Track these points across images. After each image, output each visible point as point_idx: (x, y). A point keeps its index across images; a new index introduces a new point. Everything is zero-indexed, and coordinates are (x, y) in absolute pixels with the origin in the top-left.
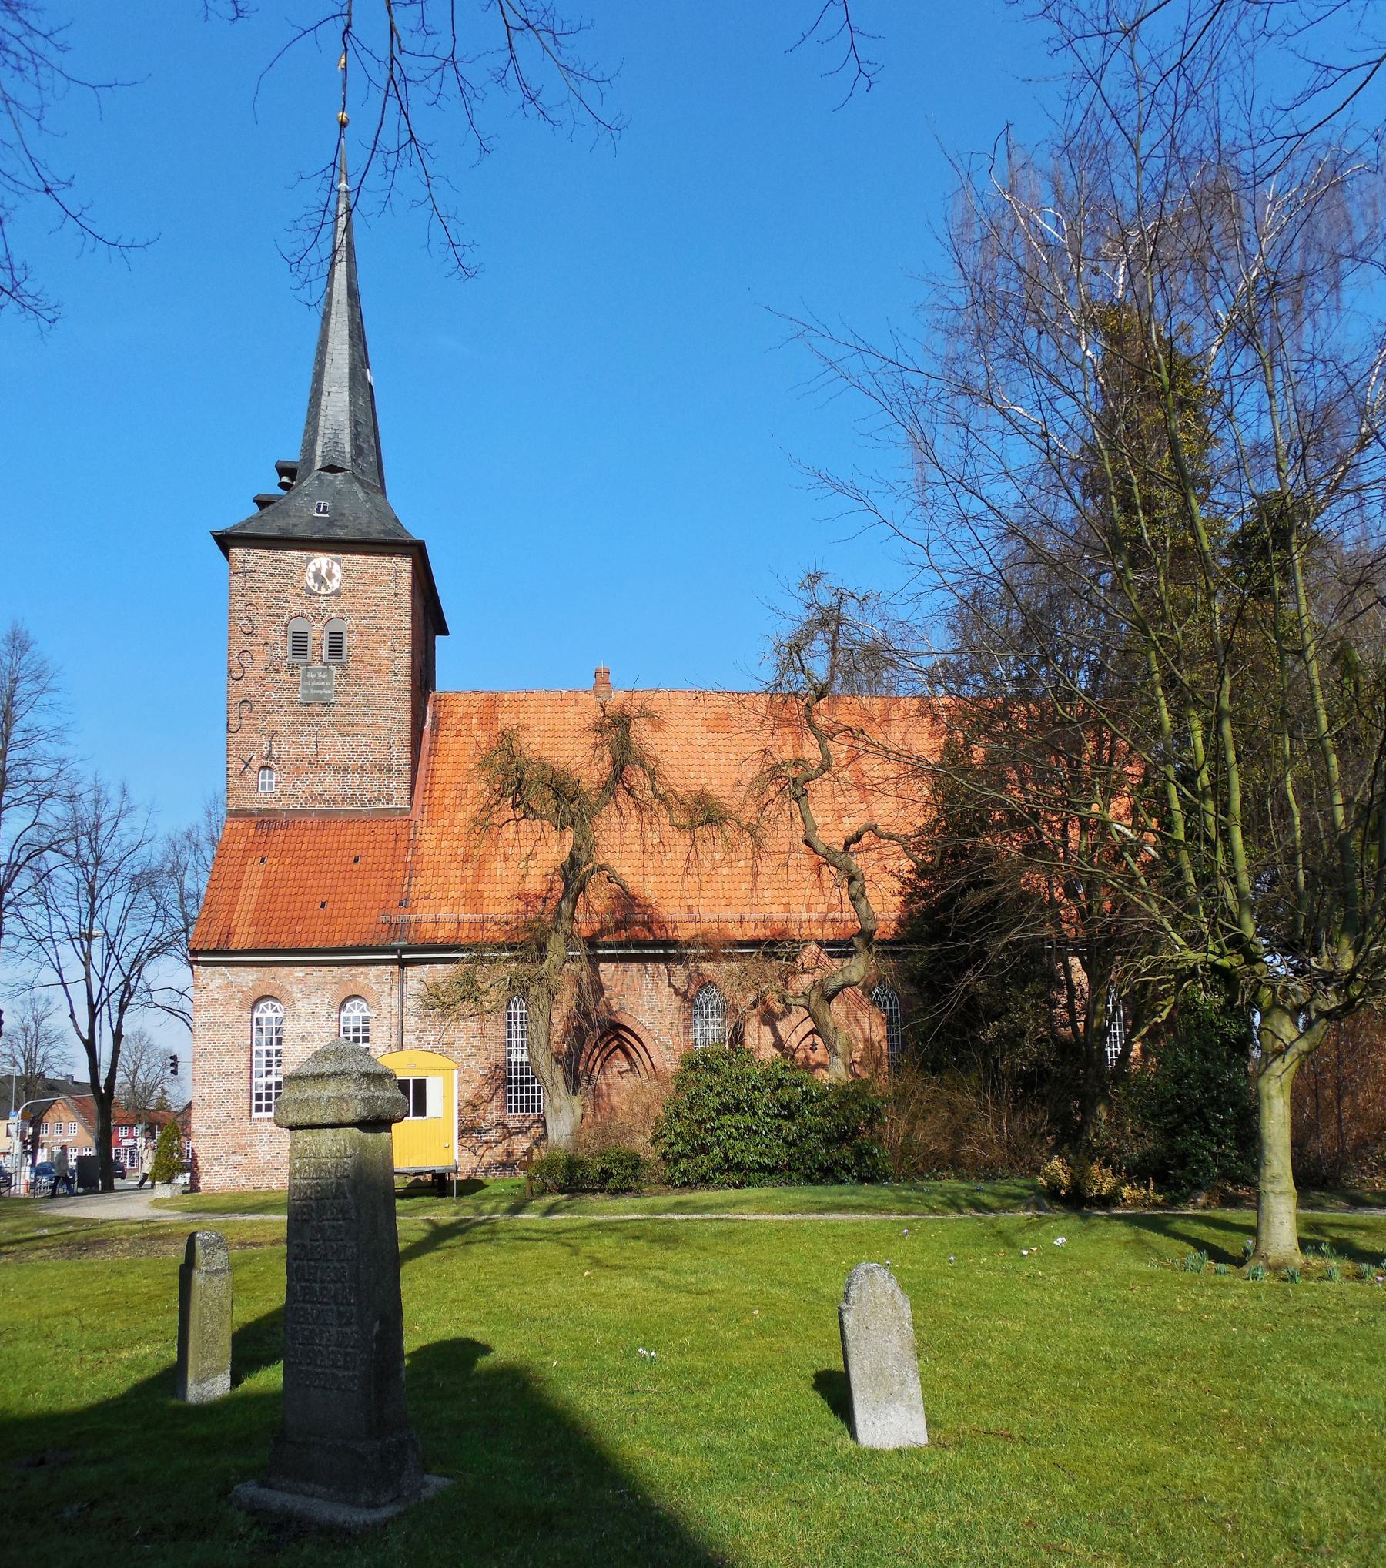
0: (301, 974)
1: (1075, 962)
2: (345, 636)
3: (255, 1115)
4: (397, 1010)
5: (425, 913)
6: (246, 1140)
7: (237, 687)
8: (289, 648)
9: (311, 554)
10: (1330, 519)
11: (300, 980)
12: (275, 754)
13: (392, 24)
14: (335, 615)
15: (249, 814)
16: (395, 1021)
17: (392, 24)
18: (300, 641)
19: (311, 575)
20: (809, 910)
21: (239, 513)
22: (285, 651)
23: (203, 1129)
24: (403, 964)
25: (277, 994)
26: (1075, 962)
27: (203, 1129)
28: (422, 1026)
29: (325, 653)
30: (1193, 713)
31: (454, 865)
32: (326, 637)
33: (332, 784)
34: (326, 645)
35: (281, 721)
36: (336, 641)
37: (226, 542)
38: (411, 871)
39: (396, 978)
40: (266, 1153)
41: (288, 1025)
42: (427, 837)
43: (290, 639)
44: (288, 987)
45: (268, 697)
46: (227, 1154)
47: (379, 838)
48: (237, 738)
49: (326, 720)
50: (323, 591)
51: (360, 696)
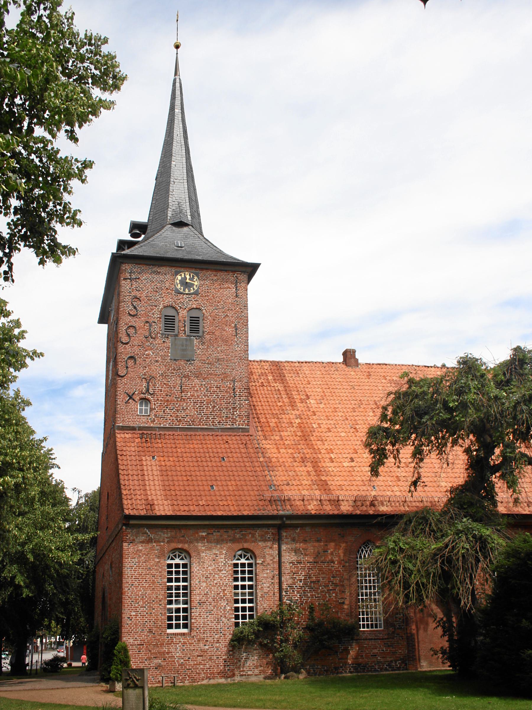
0: (204, 534)
2: (201, 319)
4: (277, 559)
7: (125, 348)
8: (162, 325)
9: (178, 269)
13: (177, 57)
14: (195, 306)
15: (133, 429)
16: (276, 566)
17: (177, 57)
18: (169, 322)
19: (178, 282)
21: (57, 469)
22: (159, 327)
23: (131, 641)
24: (280, 528)
27: (131, 641)
29: (187, 329)
30: (478, 423)
31: (295, 464)
32: (187, 320)
34: (188, 324)
36: (195, 324)
37: (59, 468)
42: (268, 446)
43: (163, 320)
45: (148, 355)
50: (187, 291)
51: (213, 356)
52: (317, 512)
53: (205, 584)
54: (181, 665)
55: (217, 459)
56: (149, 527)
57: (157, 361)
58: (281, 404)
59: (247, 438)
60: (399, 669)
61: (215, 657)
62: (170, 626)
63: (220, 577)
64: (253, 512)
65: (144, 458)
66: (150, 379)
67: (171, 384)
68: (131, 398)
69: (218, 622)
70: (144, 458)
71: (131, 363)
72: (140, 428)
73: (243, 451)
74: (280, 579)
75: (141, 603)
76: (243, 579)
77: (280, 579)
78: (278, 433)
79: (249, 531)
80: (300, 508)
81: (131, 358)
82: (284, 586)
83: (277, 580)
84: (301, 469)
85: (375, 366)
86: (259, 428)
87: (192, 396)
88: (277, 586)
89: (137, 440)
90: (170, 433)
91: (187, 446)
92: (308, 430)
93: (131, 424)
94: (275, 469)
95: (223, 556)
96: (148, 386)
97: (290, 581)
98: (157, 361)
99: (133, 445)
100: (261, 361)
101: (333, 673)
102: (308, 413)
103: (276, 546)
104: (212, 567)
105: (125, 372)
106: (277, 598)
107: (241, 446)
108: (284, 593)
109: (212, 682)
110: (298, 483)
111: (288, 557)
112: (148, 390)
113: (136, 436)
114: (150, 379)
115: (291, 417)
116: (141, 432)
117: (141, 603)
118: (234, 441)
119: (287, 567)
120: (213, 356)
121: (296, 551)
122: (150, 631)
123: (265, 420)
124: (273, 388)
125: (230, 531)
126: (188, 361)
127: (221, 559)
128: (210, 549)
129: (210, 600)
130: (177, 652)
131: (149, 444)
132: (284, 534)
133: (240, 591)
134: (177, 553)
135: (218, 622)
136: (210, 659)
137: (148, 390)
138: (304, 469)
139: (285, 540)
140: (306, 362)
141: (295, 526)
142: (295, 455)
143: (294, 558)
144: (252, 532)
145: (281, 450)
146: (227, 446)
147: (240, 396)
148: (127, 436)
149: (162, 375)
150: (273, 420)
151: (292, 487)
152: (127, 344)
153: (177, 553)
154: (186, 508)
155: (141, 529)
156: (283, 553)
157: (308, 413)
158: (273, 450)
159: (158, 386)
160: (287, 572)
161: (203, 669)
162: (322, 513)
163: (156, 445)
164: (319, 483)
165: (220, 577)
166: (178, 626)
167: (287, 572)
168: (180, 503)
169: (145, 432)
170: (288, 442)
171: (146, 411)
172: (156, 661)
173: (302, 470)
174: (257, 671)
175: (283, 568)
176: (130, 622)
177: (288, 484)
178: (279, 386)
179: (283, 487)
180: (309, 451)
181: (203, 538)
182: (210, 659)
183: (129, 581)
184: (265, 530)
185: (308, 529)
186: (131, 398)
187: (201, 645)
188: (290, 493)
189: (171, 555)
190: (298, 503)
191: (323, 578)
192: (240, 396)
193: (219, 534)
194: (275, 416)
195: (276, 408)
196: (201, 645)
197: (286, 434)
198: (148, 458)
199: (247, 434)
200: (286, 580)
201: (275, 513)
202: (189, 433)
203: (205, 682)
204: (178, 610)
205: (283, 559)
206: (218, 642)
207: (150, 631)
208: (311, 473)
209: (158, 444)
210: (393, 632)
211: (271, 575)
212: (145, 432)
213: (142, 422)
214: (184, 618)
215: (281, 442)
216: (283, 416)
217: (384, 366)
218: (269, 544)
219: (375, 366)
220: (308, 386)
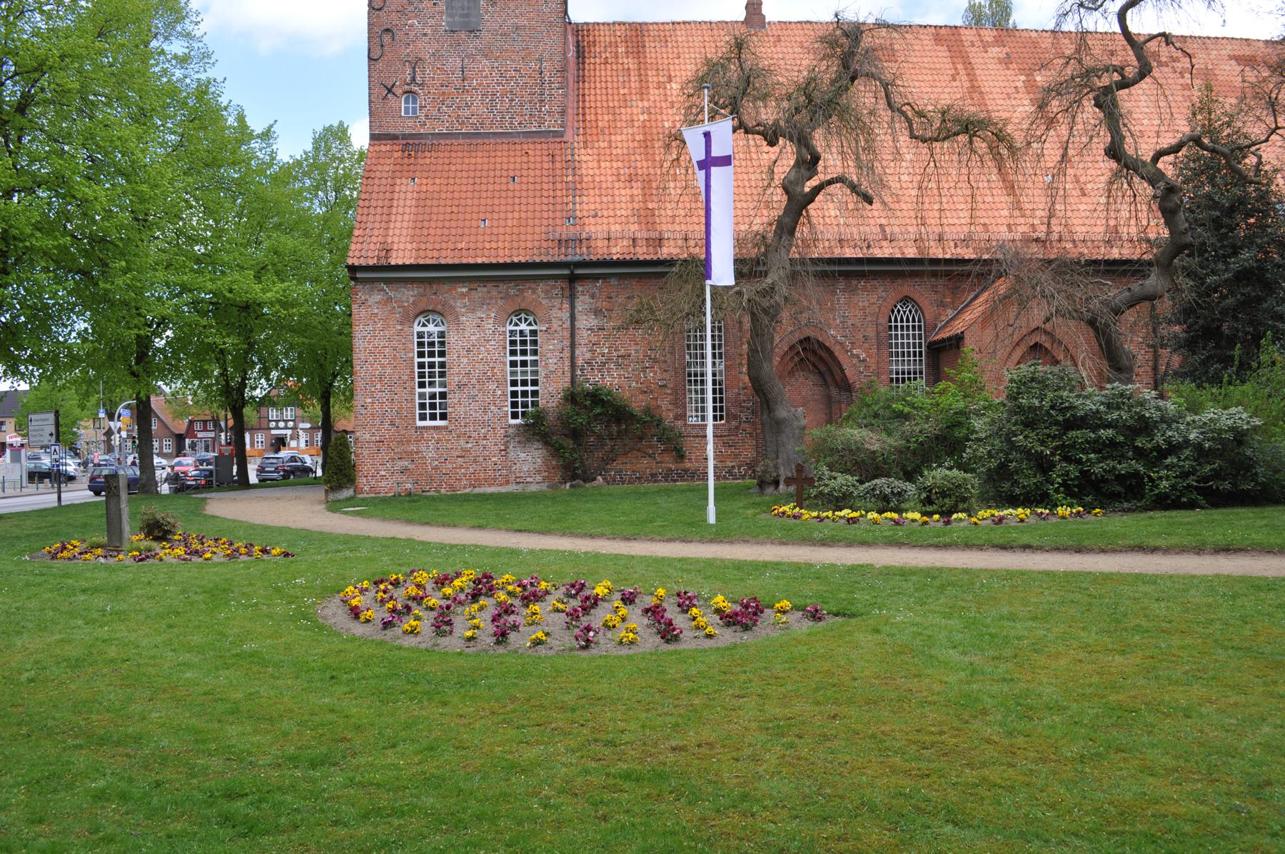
0: (464, 290)
1: (712, 519)
3: (420, 423)
4: (568, 324)
5: (594, 229)
6: (413, 448)
7: (378, 16)
10: (121, 472)
11: (463, 295)
12: (418, 79)
15: (394, 137)
16: (567, 334)
20: (1010, 231)
23: (367, 436)
24: (573, 279)
25: (439, 307)
26: (712, 519)
27: (367, 436)
28: (594, 339)
31: (617, 185)
33: (479, 107)
35: (425, 49)
38: (575, 189)
39: (567, 293)
40: (433, 459)
41: (452, 338)
44: (452, 302)
46: (393, 460)
47: (532, 159)
48: (380, 65)
49: (472, 45)
52: (621, 257)
53: (466, 360)
54: (436, 468)
55: (504, 180)
56: (388, 281)
57: (425, 35)
58: (626, 91)
59: (558, 146)
60: (743, 477)
61: (481, 459)
62: (423, 417)
63: (488, 352)
64: (528, 258)
65: (398, 181)
66: (416, 63)
67: (448, 67)
68: (390, 91)
69: (485, 412)
70: (398, 181)
71: (387, 39)
72: (405, 136)
73: (546, 166)
74: (573, 353)
75: (378, 386)
76: (524, 353)
77: (573, 353)
78: (607, 138)
79: (528, 285)
80: (601, 251)
81: (387, 30)
82: (580, 362)
83: (567, 354)
84: (623, 192)
85: (794, 26)
86: (581, 131)
87: (480, 85)
88: (567, 363)
89: (396, 155)
90: (448, 142)
91: (467, 161)
92: (655, 131)
93: (392, 131)
94: (585, 193)
95: (491, 321)
96: (414, 72)
97: (588, 355)
98: (425, 35)
99: (388, 161)
100: (614, 23)
101: (649, 481)
102: (664, 105)
103: (566, 306)
104: (477, 337)
105: (379, 53)
106: (568, 379)
107: (546, 159)
108: (579, 372)
109: (477, 490)
110: (611, 213)
111: (584, 322)
112: (414, 79)
113: (397, 148)
114: (416, 63)
115: (635, 111)
116: (404, 142)
117: (378, 386)
118: (537, 152)
119: (583, 336)
120: (509, 23)
121: (597, 312)
122: (392, 424)
123: (593, 117)
124: (620, 67)
125: (501, 285)
126: (471, 32)
127: (489, 325)
128: (473, 311)
129: (473, 381)
130: (429, 452)
131: (412, 160)
132: (580, 289)
133: (519, 369)
134: (523, 315)
135: (485, 412)
136: (475, 461)
137: (414, 79)
138: (628, 191)
139: (582, 298)
140: (684, 23)
141: (596, 278)
142: (622, 172)
143: (593, 322)
144: (533, 286)
145: (603, 165)
146: (525, 159)
147: (551, 83)
148: (383, 148)
149: (434, 55)
150: (606, 118)
151: (599, 221)
152: (380, 9)
153: (523, 315)
154: (436, 254)
155: (376, 284)
156: (578, 316)
157: (664, 105)
158: (590, 165)
159: (428, 73)
160: (583, 342)
161: (465, 475)
162: (628, 258)
163: (421, 161)
164: (642, 212)
165: (488, 352)
166: (433, 417)
167: (583, 342)
168: (430, 246)
169: (411, 142)
170: (619, 151)
171: (414, 110)
172: (401, 463)
173: (623, 193)
174: (539, 478)
175: (577, 337)
176: (364, 412)
177: (595, 216)
178: (631, 63)
179: (587, 221)
180: (645, 164)
181: (463, 295)
182: (475, 461)
183: (362, 356)
184: (551, 283)
185: (614, 281)
186: (390, 91)
187: (462, 442)
188: (593, 229)
189: (515, 319)
190: (599, 244)
191: (637, 351)
192: (551, 83)
193: (485, 289)
194: (612, 111)
195: (616, 98)
196: (462, 442)
197: (619, 138)
198: (404, 181)
199: (558, 140)
200: (582, 354)
201: (563, 258)
202: (474, 142)
203: (467, 490)
204: (433, 396)
205: (578, 324)
206: (485, 438)
207: (392, 424)
208: (636, 199)
209: (426, 159)
210: (737, 428)
211: (559, 347)
212: (411, 142)
213: (409, 127)
214: (436, 407)
215: (608, 151)
216: (623, 110)
217: (808, 26)
218: (557, 303)
219: (794, 26)
220: (676, 61)
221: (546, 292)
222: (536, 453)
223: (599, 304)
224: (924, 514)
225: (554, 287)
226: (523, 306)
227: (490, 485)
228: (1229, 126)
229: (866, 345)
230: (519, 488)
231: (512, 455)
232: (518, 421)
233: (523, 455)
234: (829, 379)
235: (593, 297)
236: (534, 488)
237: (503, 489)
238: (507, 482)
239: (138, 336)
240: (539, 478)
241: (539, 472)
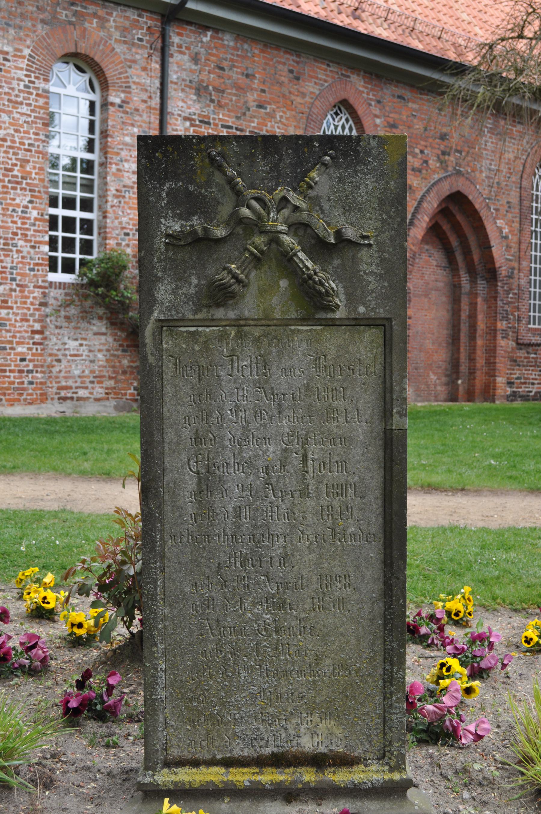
4: (156, 102)
95: (23, 64)
144: (101, 12)
156: (172, 92)
185: (228, 40)
218: (140, 55)
221: (124, 30)
222: (98, 342)
223: (204, 76)
224: (487, 425)
225: (135, 25)
226: (83, 48)
227: (12, 403)
228: (38, 429)
229: (510, 216)
230: (67, 408)
231: (53, 343)
232: (59, 277)
233: (72, 344)
234: (459, 258)
235: (195, 59)
236: (90, 410)
237: (30, 411)
238: (44, 398)
239: (494, 401)
240: (99, 391)
241: (99, 379)
